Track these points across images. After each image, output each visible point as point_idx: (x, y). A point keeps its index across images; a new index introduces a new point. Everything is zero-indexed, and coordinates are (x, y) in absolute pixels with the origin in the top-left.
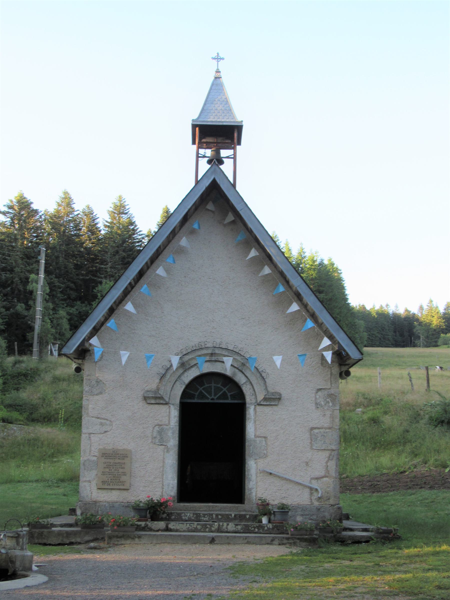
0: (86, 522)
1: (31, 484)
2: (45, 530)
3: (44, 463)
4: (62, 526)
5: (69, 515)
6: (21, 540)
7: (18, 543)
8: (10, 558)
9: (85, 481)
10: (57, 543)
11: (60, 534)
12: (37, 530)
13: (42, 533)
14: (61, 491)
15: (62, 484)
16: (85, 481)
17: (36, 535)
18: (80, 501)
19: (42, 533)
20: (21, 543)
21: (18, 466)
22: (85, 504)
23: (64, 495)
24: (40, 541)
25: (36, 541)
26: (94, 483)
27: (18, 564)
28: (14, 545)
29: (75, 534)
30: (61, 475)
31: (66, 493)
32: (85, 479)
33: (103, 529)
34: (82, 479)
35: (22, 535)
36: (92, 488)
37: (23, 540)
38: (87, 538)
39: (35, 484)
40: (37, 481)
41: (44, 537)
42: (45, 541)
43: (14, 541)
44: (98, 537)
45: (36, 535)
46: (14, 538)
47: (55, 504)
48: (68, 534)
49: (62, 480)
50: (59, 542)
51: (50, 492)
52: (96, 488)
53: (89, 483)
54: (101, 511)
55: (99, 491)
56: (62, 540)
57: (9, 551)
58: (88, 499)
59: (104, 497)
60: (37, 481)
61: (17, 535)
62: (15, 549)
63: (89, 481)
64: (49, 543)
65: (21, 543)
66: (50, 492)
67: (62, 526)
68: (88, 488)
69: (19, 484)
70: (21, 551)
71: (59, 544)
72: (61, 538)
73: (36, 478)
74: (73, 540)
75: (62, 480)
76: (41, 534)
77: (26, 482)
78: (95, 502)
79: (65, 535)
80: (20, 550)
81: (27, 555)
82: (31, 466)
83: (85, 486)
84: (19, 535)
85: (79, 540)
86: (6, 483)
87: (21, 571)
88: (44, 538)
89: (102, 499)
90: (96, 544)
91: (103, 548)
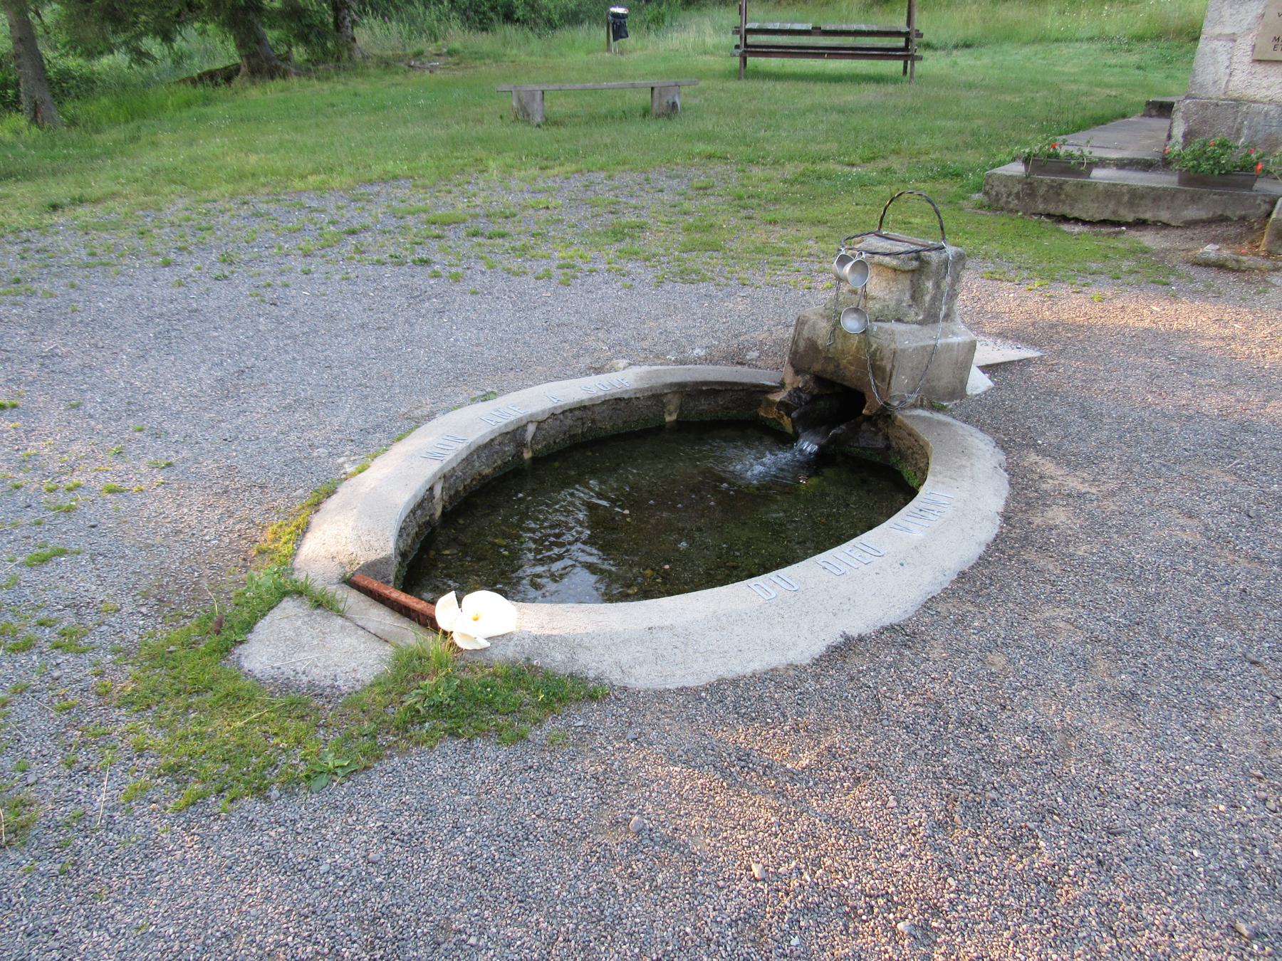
0: (1199, 165)
1: (1078, 45)
2: (1071, 180)
3: (1111, 6)
4: (1122, 164)
5: (1144, 116)
6: (930, 284)
7: (916, 296)
8: (873, 355)
9: (1218, 37)
10: (1098, 217)
11: (1111, 193)
12: (1047, 179)
13: (1061, 186)
14: (1134, 58)
15: (1137, 47)
16: (1218, 37)
17: (1042, 191)
18: (1187, 98)
19: (1061, 186)
20: (927, 298)
21: (1062, 13)
22: (1204, 107)
23: (1139, 68)
24: (1052, 208)
25: (1041, 207)
26: (1245, 45)
27: (901, 383)
28: (899, 302)
29: (1156, 196)
30: (1139, 26)
31: (1143, 64)
32: (1217, 30)
33: (1250, 188)
34: (1207, 31)
35: (934, 266)
36: (1235, 59)
37: (937, 286)
38: (1192, 213)
39: (1085, 46)
40: (1091, 39)
41: (1063, 197)
42: (1066, 210)
43: (905, 282)
44: (1228, 213)
45: (1042, 191)
46: (901, 277)
47: (1117, 86)
48: (1135, 196)
49: (1140, 39)
50: (1106, 215)
51: (1112, 60)
52: (1247, 59)
53: (1231, 44)
54: (1249, 128)
55: (1259, 68)
56: (1114, 212)
57: (875, 326)
58: (1214, 93)
59: (1268, 88)
60: (1091, 39)
61: (915, 264)
62: (899, 320)
63: (1232, 38)
64: (1076, 215)
65: (927, 298)
66: (1112, 60)
67: (1122, 164)
68: (1223, 58)
69: (1056, 45)
70: (926, 331)
71: (1104, 222)
72: (1111, 206)
73: (1090, 35)
74: (1148, 216)
75: (1140, 39)
76: (1057, 189)
77: (1071, 41)
78: (1238, 101)
79: (1126, 198)
80: (920, 323)
81: (949, 347)
82: (1084, 13)
83: (1215, 51)
84: (923, 263)
85: (1164, 216)
86: (1034, 42)
87: (914, 406)
88: (1064, 202)
89: (1261, 94)
90: (1226, 253)
91: (1250, 270)
